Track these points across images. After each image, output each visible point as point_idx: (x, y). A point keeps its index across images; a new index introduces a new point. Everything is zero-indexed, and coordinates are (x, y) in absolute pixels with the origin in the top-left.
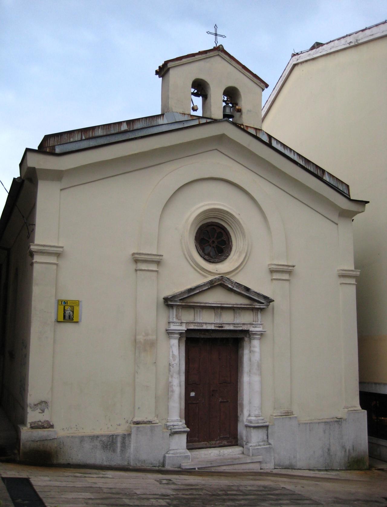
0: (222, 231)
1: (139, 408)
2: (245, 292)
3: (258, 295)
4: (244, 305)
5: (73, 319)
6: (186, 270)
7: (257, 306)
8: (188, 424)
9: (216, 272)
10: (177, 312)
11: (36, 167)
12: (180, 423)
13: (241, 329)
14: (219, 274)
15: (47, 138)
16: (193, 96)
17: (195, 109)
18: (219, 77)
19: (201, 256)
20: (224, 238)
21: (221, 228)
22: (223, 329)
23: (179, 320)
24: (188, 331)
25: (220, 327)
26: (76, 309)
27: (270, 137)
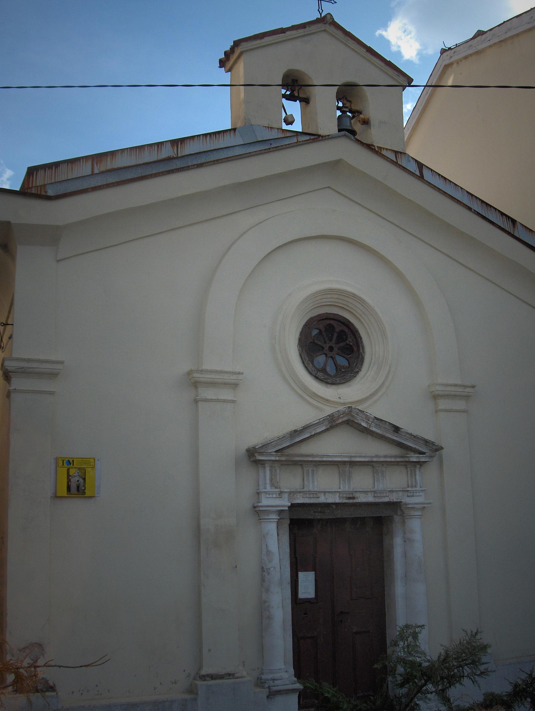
0: (346, 330)
1: (209, 650)
2: (391, 433)
3: (415, 438)
4: (391, 457)
5: (84, 493)
6: (281, 397)
7: (414, 458)
8: (299, 674)
9: (338, 400)
10: (271, 471)
11: (13, 222)
12: (285, 675)
13: (386, 500)
14: (344, 404)
15: (32, 171)
16: (284, 100)
17: (289, 121)
18: (326, 68)
19: (310, 373)
20: (350, 340)
21: (344, 324)
22: (355, 501)
23: (276, 488)
24: (293, 506)
25: (350, 498)
26: (89, 473)
27: (420, 166)
